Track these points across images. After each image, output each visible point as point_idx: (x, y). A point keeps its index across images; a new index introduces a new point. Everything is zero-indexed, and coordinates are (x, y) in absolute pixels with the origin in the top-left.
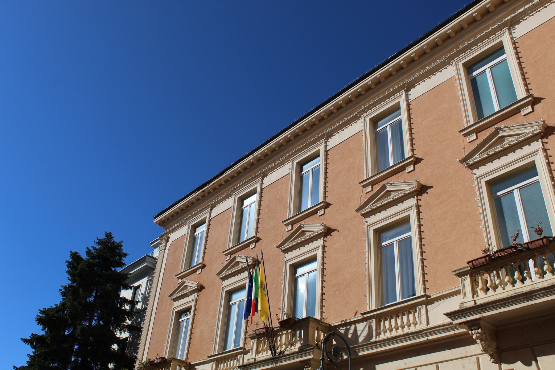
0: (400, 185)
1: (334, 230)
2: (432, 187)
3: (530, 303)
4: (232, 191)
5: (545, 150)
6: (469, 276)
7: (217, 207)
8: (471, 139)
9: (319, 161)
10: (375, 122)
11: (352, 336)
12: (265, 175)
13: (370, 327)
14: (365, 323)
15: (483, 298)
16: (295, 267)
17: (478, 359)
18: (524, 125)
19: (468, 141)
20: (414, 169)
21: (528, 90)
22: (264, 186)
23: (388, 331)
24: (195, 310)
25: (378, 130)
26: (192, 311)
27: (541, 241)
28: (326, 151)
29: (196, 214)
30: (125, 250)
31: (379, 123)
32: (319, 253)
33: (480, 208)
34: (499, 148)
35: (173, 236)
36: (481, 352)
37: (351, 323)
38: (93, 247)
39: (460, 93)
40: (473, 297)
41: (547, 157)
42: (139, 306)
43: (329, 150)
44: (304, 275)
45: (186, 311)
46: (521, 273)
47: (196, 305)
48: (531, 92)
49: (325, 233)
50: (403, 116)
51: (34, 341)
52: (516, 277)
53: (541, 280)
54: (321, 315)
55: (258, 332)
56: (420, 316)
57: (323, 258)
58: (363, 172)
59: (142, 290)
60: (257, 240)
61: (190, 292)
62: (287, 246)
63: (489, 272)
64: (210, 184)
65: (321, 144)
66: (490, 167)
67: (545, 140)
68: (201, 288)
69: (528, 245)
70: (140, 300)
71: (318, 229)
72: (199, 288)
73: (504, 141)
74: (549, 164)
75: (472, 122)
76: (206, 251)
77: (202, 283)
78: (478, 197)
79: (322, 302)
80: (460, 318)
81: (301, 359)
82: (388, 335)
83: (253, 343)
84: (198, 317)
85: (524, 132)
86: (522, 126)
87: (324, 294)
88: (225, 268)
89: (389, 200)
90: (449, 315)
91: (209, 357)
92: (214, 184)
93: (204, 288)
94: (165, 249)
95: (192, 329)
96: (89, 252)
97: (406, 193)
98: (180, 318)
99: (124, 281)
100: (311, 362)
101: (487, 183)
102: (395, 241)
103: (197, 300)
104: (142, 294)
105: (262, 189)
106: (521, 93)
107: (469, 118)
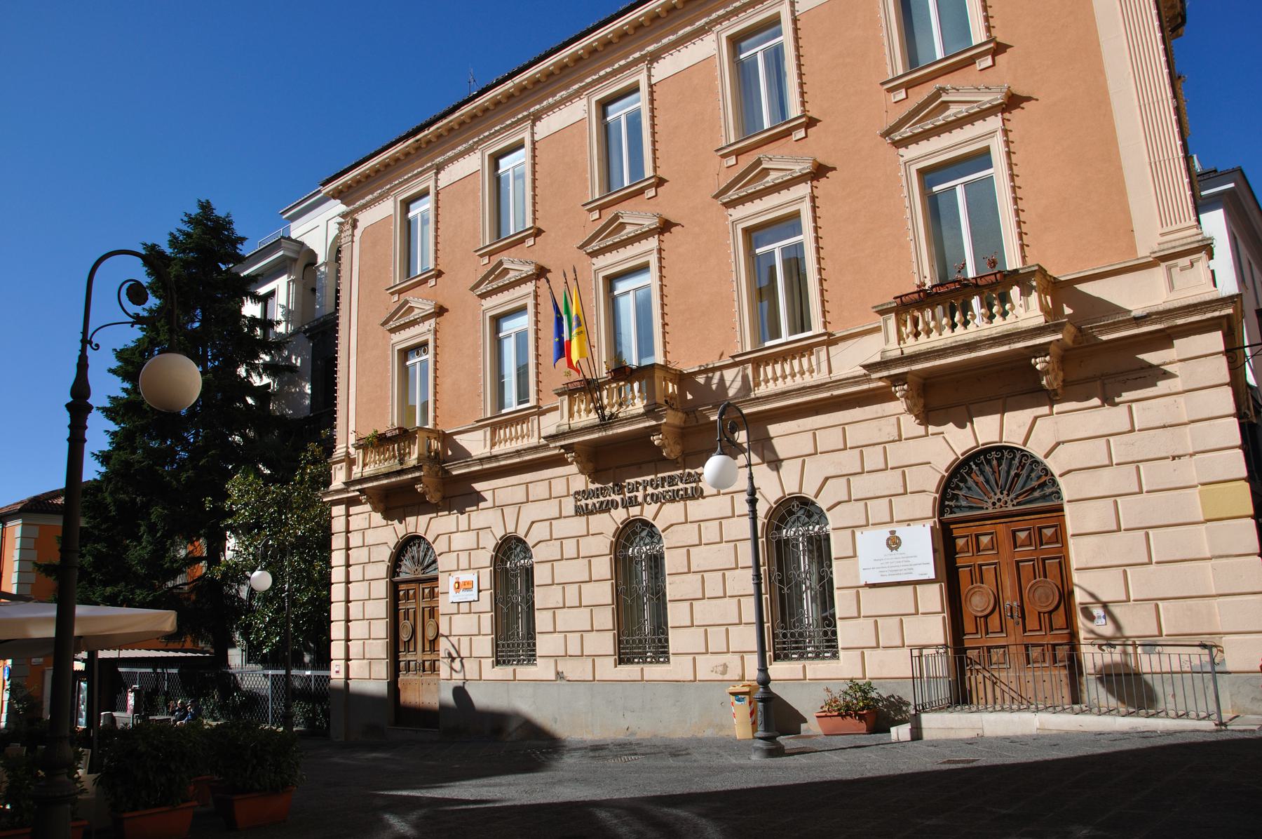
1: (676, 225)
2: (834, 169)
3: (973, 355)
5: (1006, 132)
7: (447, 169)
9: (638, 100)
13: (745, 378)
14: (736, 370)
15: (912, 346)
16: (497, 321)
17: (898, 419)
22: (537, 138)
24: (436, 347)
25: (742, 56)
28: (651, 86)
29: (407, 181)
30: (239, 230)
31: (743, 44)
33: (908, 211)
34: (940, 121)
37: (714, 369)
38: (179, 230)
39: (882, 15)
41: (1007, 143)
44: (628, 292)
45: (421, 347)
46: (964, 314)
47: (435, 340)
52: (956, 320)
53: (989, 326)
54: (665, 356)
55: (571, 387)
56: (819, 364)
57: (661, 268)
59: (281, 298)
62: (595, 246)
63: (921, 310)
64: (432, 129)
67: (1007, 115)
68: (440, 311)
71: (650, 223)
73: (948, 108)
74: (1009, 154)
75: (900, 72)
76: (439, 247)
78: (906, 193)
79: (664, 337)
84: (444, 358)
90: (864, 367)
93: (447, 310)
95: (436, 378)
96: (174, 241)
99: (245, 288)
101: (921, 172)
102: (777, 248)
104: (283, 307)
106: (978, 35)
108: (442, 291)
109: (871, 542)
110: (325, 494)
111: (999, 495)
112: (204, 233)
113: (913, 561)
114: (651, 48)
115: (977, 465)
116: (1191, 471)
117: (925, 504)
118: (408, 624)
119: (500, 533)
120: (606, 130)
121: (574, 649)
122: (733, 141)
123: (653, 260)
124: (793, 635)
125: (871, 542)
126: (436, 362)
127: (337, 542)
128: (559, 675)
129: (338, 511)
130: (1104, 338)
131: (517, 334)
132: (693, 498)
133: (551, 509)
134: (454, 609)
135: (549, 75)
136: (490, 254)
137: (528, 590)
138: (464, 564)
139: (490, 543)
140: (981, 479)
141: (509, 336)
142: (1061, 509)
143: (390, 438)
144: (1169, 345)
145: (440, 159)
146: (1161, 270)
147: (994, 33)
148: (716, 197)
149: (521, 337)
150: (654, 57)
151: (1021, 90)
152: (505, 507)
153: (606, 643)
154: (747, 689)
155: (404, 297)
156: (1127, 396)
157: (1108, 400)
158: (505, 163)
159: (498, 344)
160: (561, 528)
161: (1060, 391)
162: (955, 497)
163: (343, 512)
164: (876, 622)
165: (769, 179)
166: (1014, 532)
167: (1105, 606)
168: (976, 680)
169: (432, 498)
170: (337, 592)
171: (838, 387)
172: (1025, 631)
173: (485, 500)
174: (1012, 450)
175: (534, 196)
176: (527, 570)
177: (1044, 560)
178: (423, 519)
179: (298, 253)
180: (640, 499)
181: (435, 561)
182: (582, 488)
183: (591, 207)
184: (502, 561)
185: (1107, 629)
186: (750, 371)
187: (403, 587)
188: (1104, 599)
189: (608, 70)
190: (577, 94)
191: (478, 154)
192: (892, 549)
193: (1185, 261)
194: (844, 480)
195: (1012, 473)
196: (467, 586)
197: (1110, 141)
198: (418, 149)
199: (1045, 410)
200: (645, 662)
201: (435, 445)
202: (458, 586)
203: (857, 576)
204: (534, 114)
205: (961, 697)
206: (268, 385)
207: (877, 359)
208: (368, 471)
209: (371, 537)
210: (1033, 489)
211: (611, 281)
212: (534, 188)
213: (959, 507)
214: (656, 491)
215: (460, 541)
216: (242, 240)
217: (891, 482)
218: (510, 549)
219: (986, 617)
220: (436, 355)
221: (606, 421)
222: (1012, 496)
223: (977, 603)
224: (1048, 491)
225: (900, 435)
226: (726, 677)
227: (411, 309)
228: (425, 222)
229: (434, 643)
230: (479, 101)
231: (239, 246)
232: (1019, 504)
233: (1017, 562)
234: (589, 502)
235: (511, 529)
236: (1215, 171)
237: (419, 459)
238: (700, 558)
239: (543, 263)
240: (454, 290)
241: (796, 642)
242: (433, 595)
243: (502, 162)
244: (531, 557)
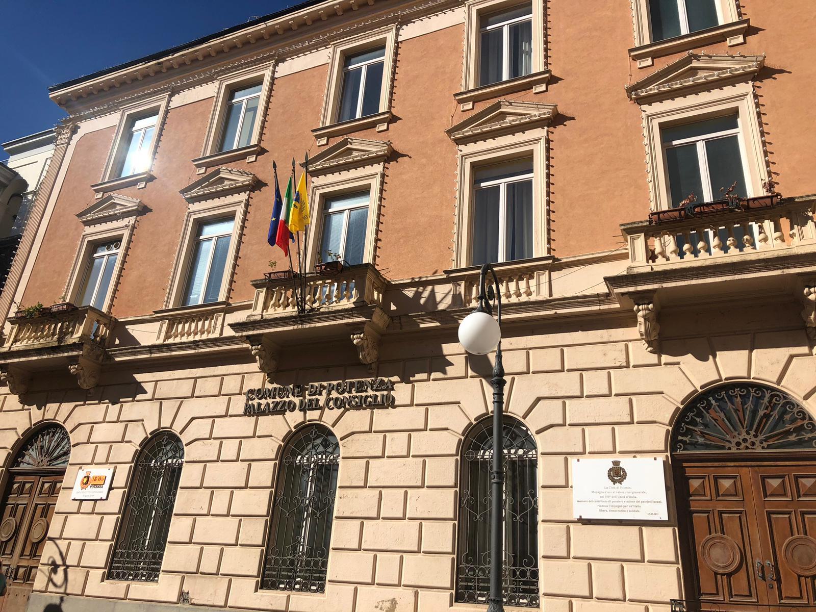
0: (366, 144)
2: (573, 118)
3: (737, 277)
4: (217, 73)
6: (643, 234)
7: (182, 94)
8: (644, 64)
10: (348, 57)
11: (426, 302)
12: (281, 59)
16: (200, 224)
18: (733, 57)
19: (639, 66)
20: (546, 91)
21: (546, 64)
22: (276, 75)
23: (206, 333)
26: (124, 243)
27: (769, 200)
28: (397, 42)
31: (353, 60)
34: (690, 82)
35: (87, 127)
36: (259, 370)
40: (262, 312)
43: (401, 42)
44: (342, 211)
45: (115, 241)
48: (550, 67)
49: (140, 212)
50: (387, 59)
56: (538, 285)
58: (460, 81)
61: (123, 213)
64: (176, 55)
65: (389, 30)
66: (481, 145)
69: (748, 203)
72: (140, 209)
75: (472, 87)
77: (146, 202)
80: (626, 286)
81: (350, 320)
82: (178, 340)
83: (258, 294)
84: (135, 252)
85: (731, 66)
86: (730, 58)
87: (380, 240)
88: (198, 184)
89: (504, 125)
90: (286, 256)
91: (156, 312)
92: (182, 55)
93: (151, 210)
94: (68, 144)
97: (533, 119)
100: (9, 366)
101: (473, 165)
102: (503, 184)
103: (134, 227)
105: (273, 79)
107: (469, 79)
109: (589, 474)
111: (744, 435)
113: (640, 497)
115: (717, 400)
117: (657, 437)
118: (13, 521)
119: (152, 426)
121: (209, 565)
122: (328, 124)
123: (375, 184)
124: (284, 562)
125: (589, 474)
128: (183, 597)
131: (219, 238)
132: (382, 406)
133: (217, 406)
134: (74, 507)
137: (169, 493)
138: (101, 457)
139: (137, 436)
141: (210, 239)
149: (222, 240)
151: (770, 63)
152: (166, 401)
153: (248, 561)
160: (223, 427)
161: (92, 391)
162: (689, 432)
166: (763, 478)
169: (85, 383)
173: (145, 392)
174: (760, 388)
175: (264, 122)
178: (67, 407)
179: (10, 181)
180: (321, 403)
181: (67, 453)
183: (318, 133)
186: (462, 289)
191: (217, 83)
192: (614, 482)
194: (559, 402)
195: (761, 413)
196: (97, 483)
198: (158, 73)
199: (805, 350)
200: (292, 588)
201: (103, 330)
202: (87, 481)
203: (569, 509)
210: (788, 433)
211: (327, 199)
213: (695, 445)
214: (341, 396)
215: (102, 433)
217: (616, 409)
218: (159, 445)
219: (729, 575)
221: (303, 316)
222: (761, 437)
223: (717, 557)
225: (628, 361)
232: (769, 447)
234: (263, 402)
235: (166, 423)
238: (380, 472)
241: (525, 583)
242: (53, 491)
244: (182, 457)
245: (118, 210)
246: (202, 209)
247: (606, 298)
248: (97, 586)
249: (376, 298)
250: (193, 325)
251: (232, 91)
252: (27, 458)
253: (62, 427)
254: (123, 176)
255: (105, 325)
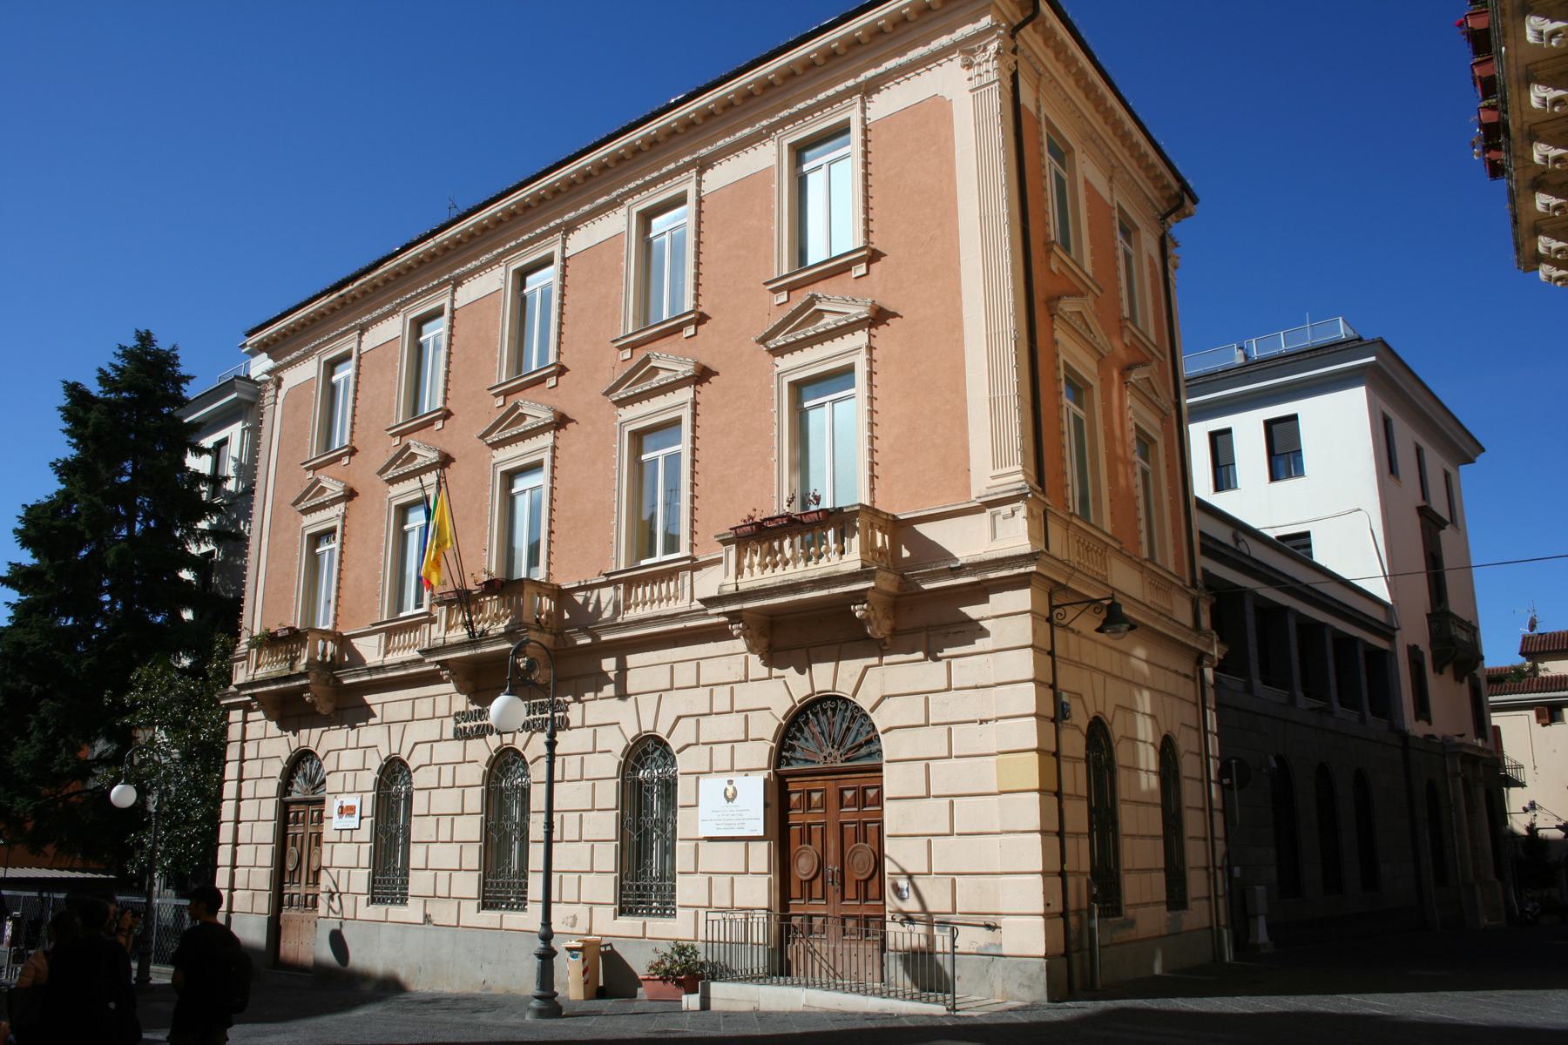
15: (749, 581)
16: (510, 477)
24: (343, 535)
29: (331, 340)
31: (808, 154)
32: (546, 457)
34: (810, 331)
42: (230, 486)
47: (343, 527)
51: (18, 578)
55: (446, 597)
57: (553, 468)
59: (233, 449)
60: (447, 415)
70: (232, 473)
77: (352, 484)
96: (104, 379)
98: (317, 546)
99: (186, 438)
102: (660, 454)
108: (565, 394)
110: (224, 696)
112: (138, 370)
114: (704, 151)
116: (991, 738)
117: (759, 754)
119: (632, 732)
120: (521, 303)
122: (786, 272)
126: (341, 553)
127: (232, 752)
129: (236, 715)
130: (926, 587)
135: (570, 184)
136: (506, 394)
139: (375, 763)
140: (817, 730)
142: (878, 769)
143: (282, 638)
144: (985, 600)
145: (364, 319)
146: (986, 516)
147: (872, 237)
148: (607, 394)
150: (570, 228)
151: (890, 305)
153: (469, 884)
154: (580, 945)
155: (406, 440)
156: (948, 652)
157: (932, 655)
158: (658, 224)
159: (509, 502)
161: (888, 640)
163: (240, 718)
164: (954, 881)
165: (823, 322)
167: (910, 876)
168: (794, 950)
169: (324, 708)
170: (227, 810)
171: (690, 619)
172: (843, 899)
175: (448, 373)
176: (523, 789)
177: (866, 823)
178: (316, 732)
181: (324, 781)
182: (463, 709)
184: (497, 778)
185: (911, 905)
186: (621, 593)
187: (293, 808)
188: (910, 871)
189: (655, 174)
190: (496, 261)
193: (1006, 509)
197: (959, 370)
198: (343, 304)
199: (875, 660)
200: (649, 914)
202: (342, 811)
204: (454, 278)
205: (780, 968)
206: (211, 553)
207: (715, 594)
208: (261, 673)
209: (267, 748)
210: (861, 746)
212: (448, 363)
216: (187, 379)
220: (342, 544)
221: (475, 640)
223: (803, 866)
224: (874, 748)
225: (746, 676)
226: (575, 930)
227: (522, 417)
228: (437, 347)
229: (317, 873)
230: (402, 259)
231: (184, 385)
232: (848, 760)
233: (842, 824)
234: (467, 725)
235: (395, 750)
236: (1360, 339)
237: (307, 664)
239: (448, 449)
240: (461, 437)
242: (321, 819)
243: (529, 279)
245: (662, 378)
246: (510, 456)
247: (418, 662)
248: (368, 912)
249: (879, 544)
250: (656, 589)
251: (799, 151)
252: (295, 787)
253: (312, 753)
254: (810, 263)
255: (880, 529)
